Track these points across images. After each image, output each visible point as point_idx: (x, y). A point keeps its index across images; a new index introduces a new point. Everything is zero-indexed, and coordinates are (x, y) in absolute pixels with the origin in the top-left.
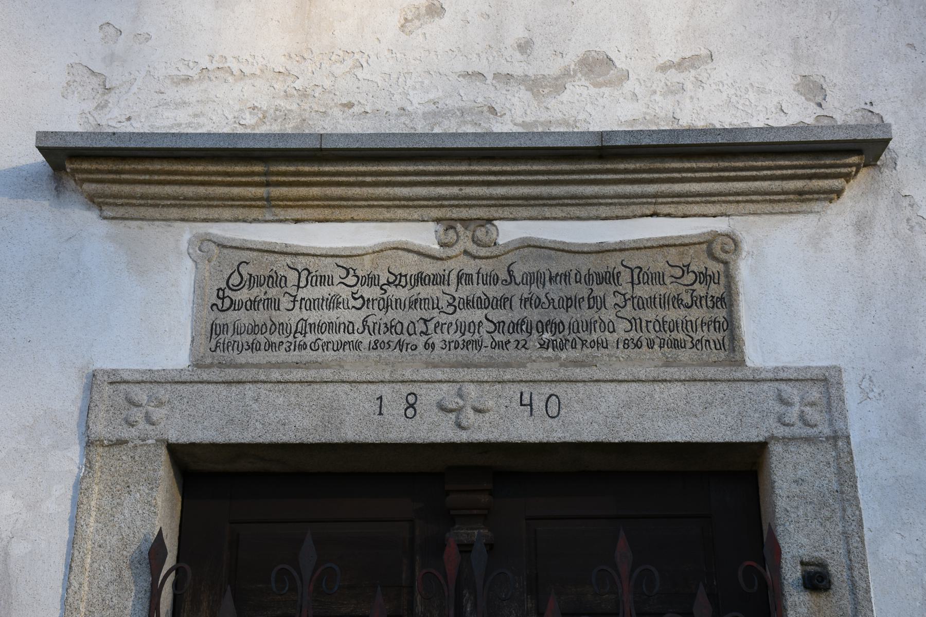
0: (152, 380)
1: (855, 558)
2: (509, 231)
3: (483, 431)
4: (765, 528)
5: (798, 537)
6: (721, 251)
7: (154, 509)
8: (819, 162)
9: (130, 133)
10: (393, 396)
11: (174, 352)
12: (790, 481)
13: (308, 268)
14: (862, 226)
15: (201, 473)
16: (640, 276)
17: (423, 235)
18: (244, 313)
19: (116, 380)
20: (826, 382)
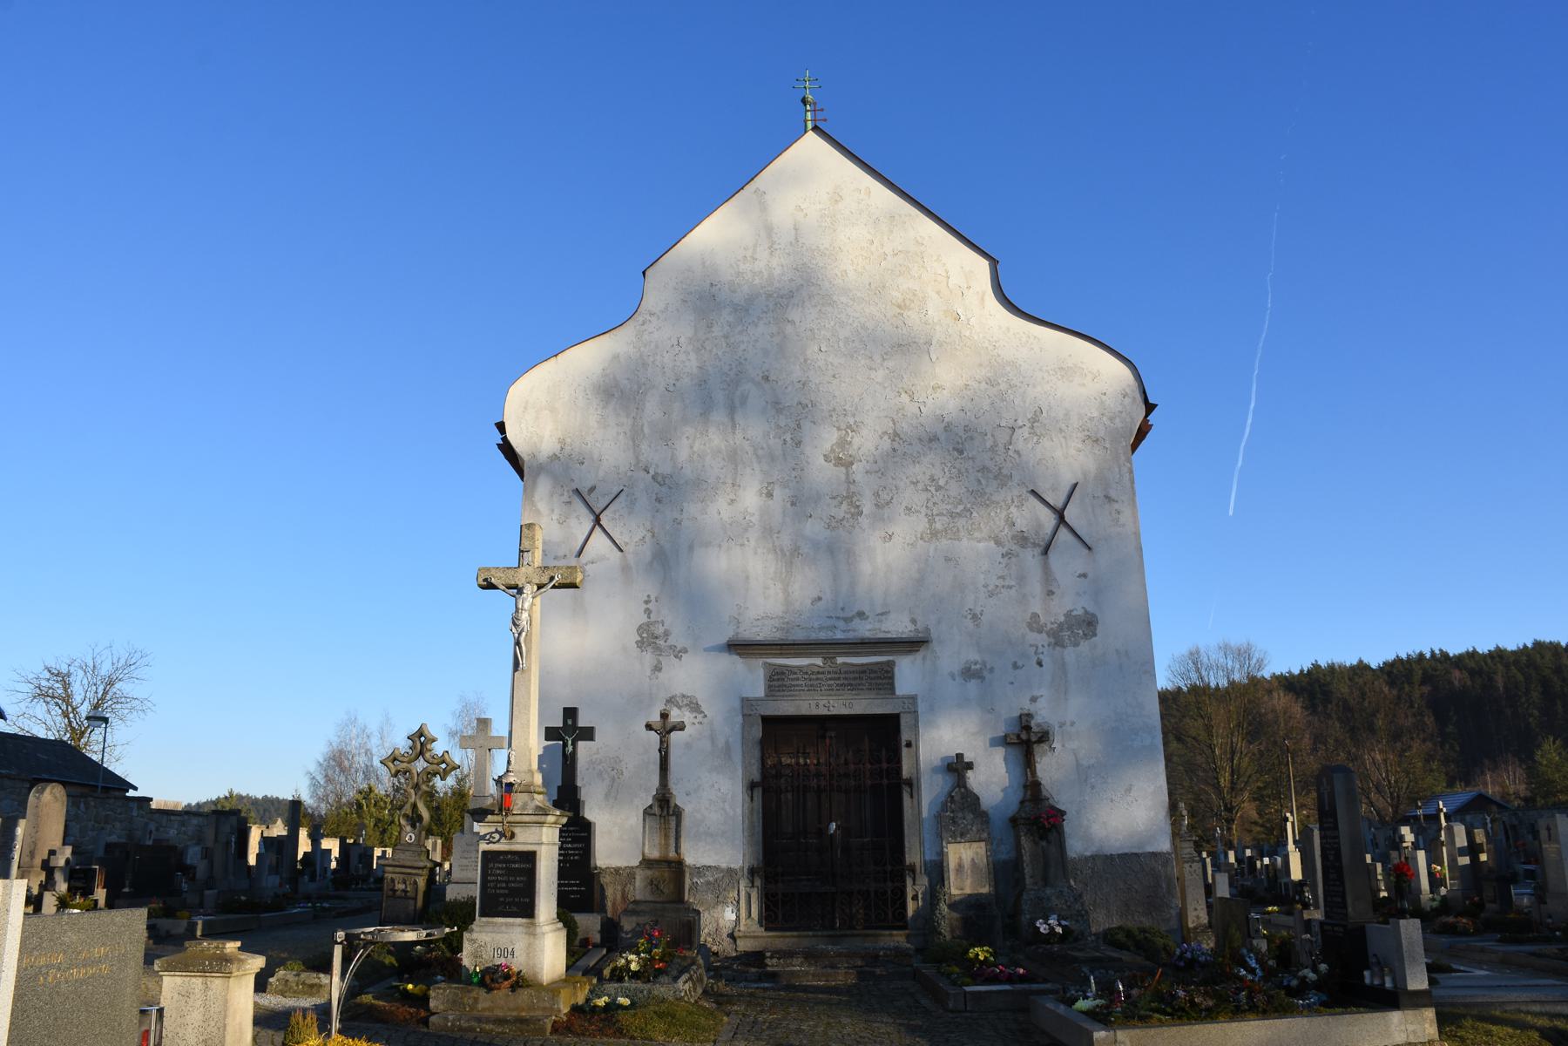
0: (757, 700)
1: (917, 740)
2: (840, 660)
3: (834, 712)
4: (596, 887)
5: (905, 736)
6: (891, 664)
7: (757, 732)
8: (913, 645)
9: (1314, 687)
10: (813, 703)
11: (760, 692)
12: (905, 721)
13: (791, 670)
14: (924, 658)
15: (767, 721)
16: (872, 671)
17: (819, 661)
18: (777, 681)
19: (748, 699)
20: (913, 698)
